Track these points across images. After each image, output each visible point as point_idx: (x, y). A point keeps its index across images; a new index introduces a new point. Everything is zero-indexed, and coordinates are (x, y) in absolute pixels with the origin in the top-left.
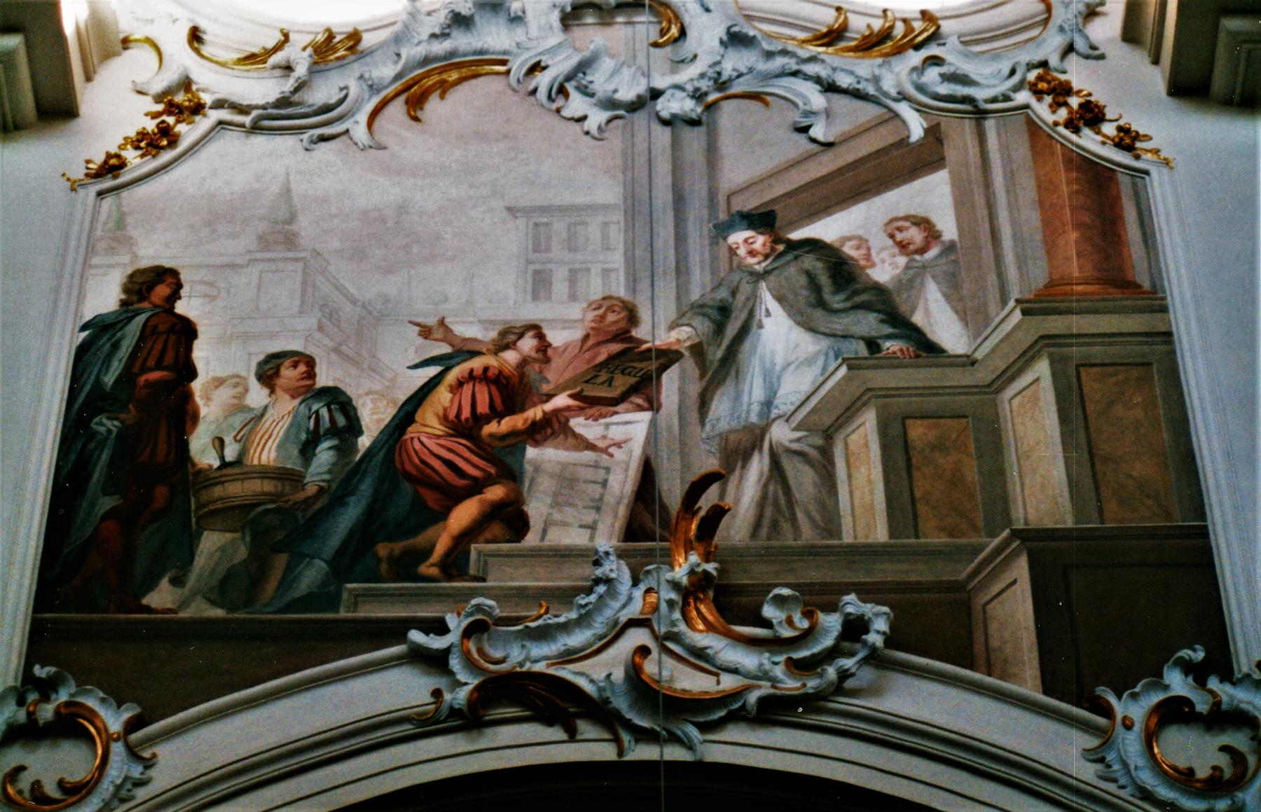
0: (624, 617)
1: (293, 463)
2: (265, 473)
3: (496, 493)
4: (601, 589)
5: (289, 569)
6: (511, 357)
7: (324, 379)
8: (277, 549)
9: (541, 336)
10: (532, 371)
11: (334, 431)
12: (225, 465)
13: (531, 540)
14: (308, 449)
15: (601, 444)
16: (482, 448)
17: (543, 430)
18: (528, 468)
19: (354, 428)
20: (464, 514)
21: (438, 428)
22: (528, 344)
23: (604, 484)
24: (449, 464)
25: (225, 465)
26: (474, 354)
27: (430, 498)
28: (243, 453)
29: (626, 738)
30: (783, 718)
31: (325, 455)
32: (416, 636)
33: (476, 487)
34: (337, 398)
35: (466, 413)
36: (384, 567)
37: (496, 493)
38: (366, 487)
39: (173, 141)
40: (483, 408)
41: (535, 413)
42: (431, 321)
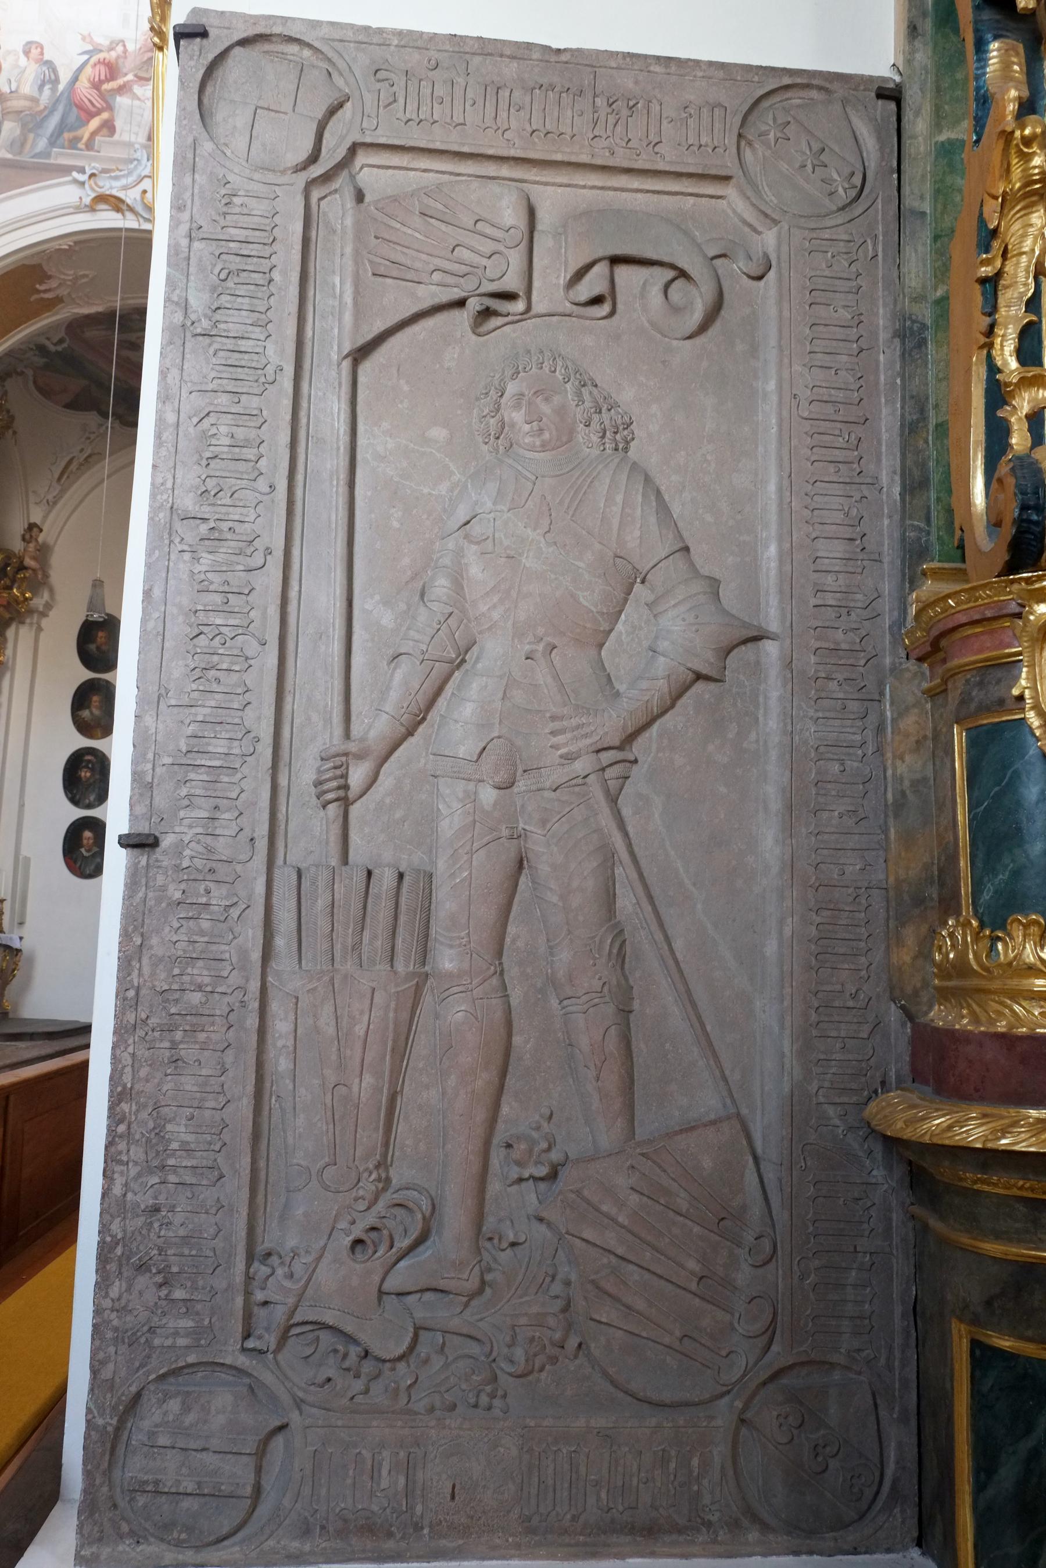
0: (143, 174)
1: (36, 94)
2: (26, 98)
3: (105, 115)
4: (136, 163)
5: (34, 140)
6: (113, 54)
7: (46, 57)
8: (30, 131)
9: (124, 46)
10: (121, 61)
11: (50, 81)
12: (11, 92)
13: (116, 137)
14: (41, 87)
15: (142, 98)
16: (102, 96)
17: (122, 89)
18: (117, 106)
19: (56, 81)
20: (95, 123)
21: (87, 85)
22: (120, 48)
23: (142, 116)
24: (90, 101)
25: (11, 92)
26: (101, 51)
27: (83, 115)
28: (18, 87)
29: (141, 220)
30: (1007, 651)
31: (47, 90)
32: (75, 174)
33: (98, 113)
34: (50, 64)
35: (97, 79)
36: (66, 143)
37: (105, 115)
38: (61, 108)
39: (905, 1122)
40: (103, 77)
41: (120, 81)
42: (86, 33)
